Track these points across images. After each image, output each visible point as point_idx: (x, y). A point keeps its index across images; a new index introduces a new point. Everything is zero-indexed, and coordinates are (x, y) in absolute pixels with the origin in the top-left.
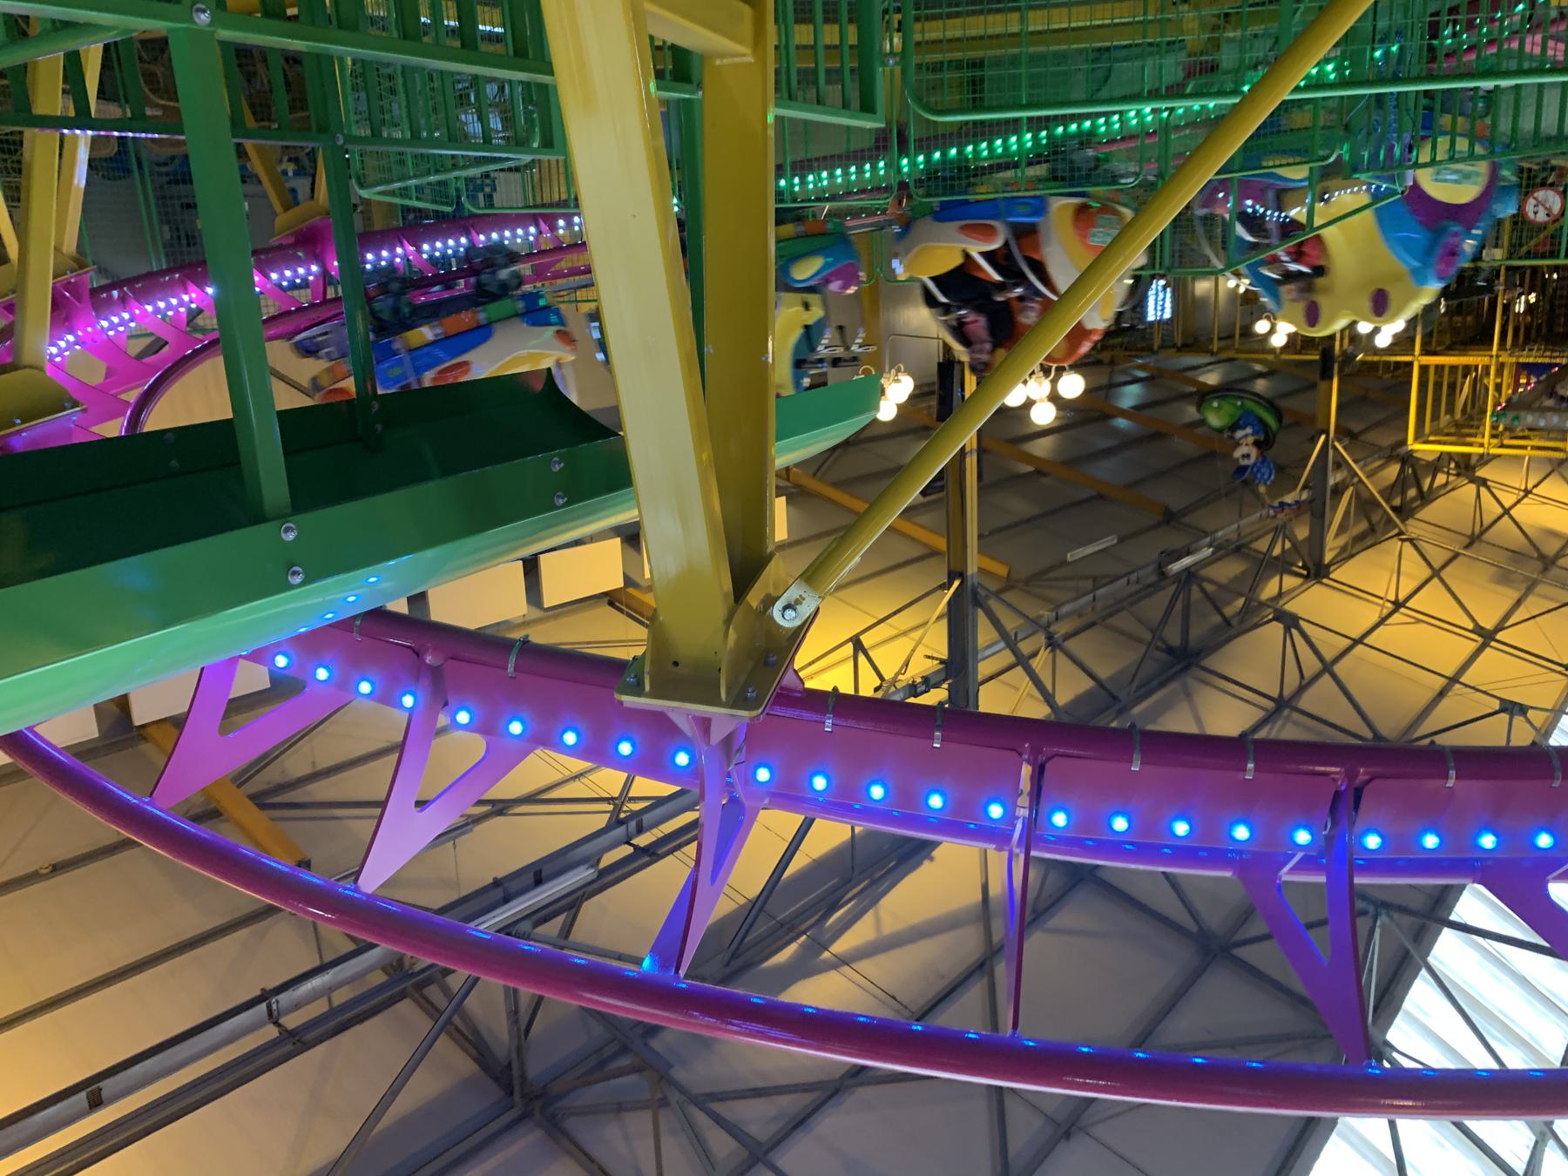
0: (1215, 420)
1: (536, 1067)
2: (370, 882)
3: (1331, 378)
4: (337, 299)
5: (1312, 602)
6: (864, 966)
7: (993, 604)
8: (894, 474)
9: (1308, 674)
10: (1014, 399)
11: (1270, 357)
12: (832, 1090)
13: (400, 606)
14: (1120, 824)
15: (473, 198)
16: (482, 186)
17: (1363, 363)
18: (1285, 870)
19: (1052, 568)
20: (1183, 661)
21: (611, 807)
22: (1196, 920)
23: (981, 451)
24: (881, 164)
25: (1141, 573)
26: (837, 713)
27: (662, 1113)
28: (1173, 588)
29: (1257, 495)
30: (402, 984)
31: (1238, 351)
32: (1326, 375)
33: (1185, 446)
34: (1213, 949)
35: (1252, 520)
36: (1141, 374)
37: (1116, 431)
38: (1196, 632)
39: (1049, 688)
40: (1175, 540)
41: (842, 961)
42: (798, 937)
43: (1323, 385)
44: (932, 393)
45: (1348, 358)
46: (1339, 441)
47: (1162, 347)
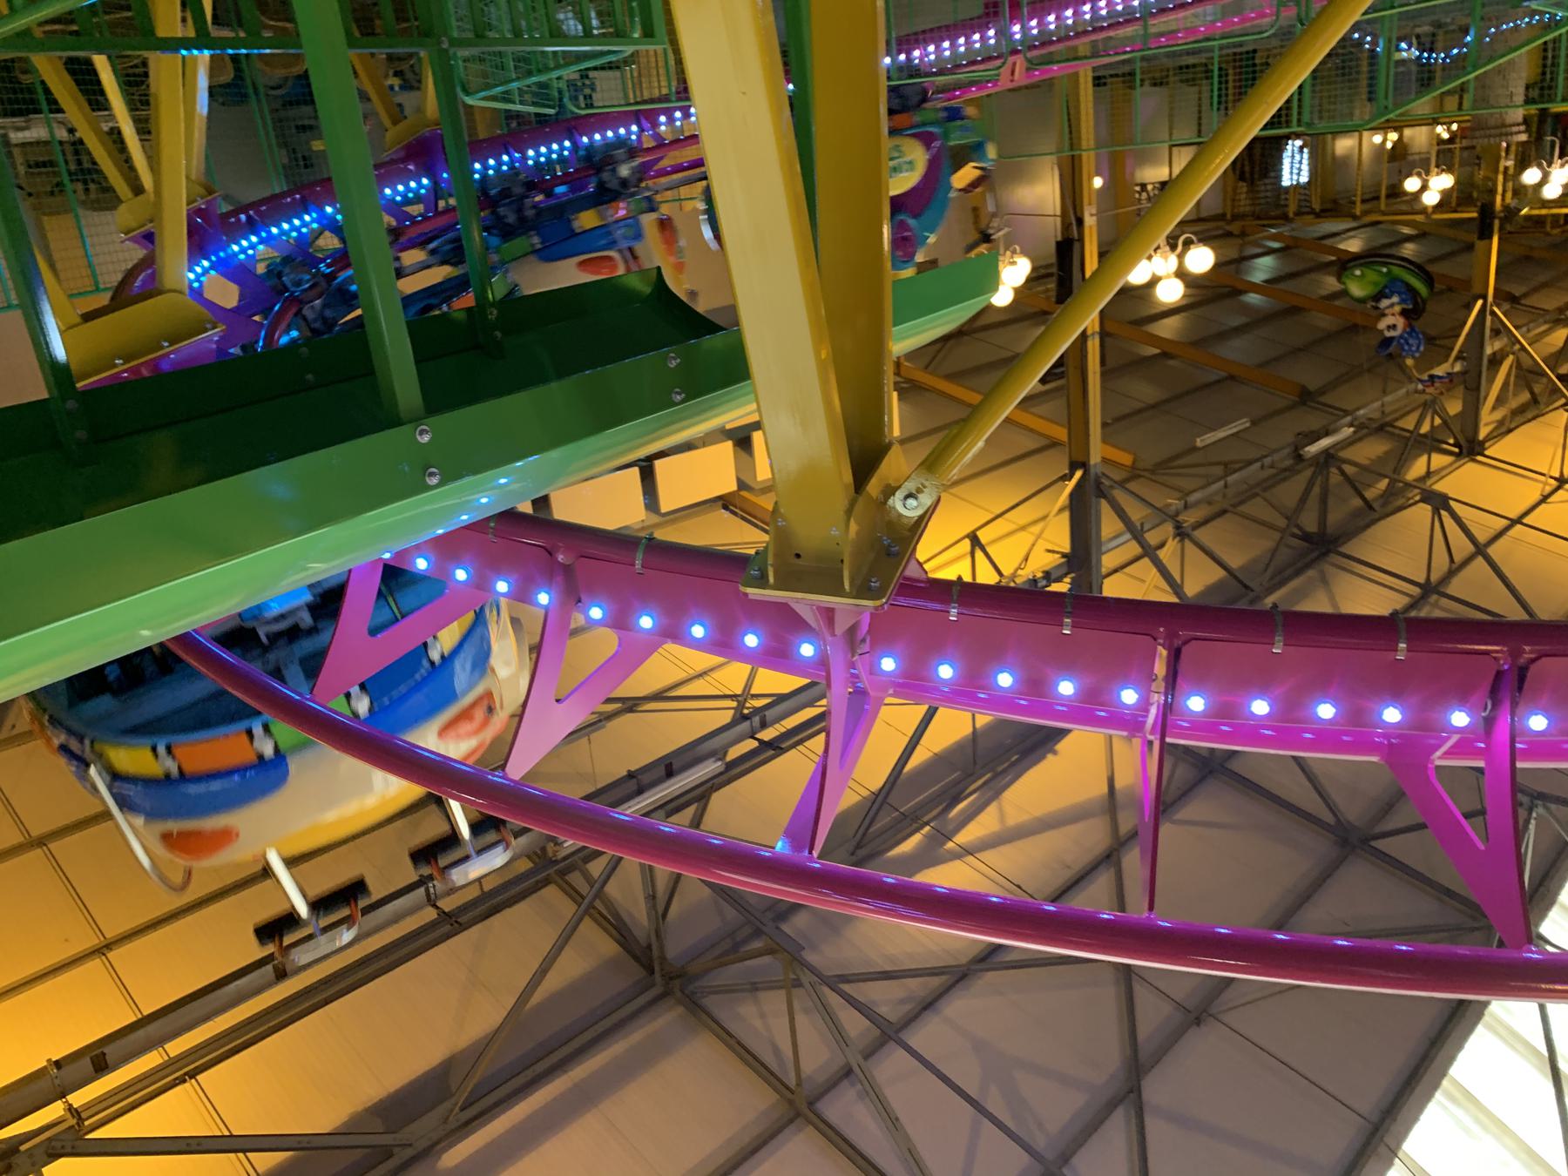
0: (1357, 290)
1: (675, 948)
2: (517, 769)
3: (1491, 238)
4: (450, 210)
5: (1465, 482)
6: (989, 856)
7: (1118, 494)
8: (1009, 363)
9: (1458, 558)
10: (1138, 275)
11: (1420, 218)
12: (958, 976)
13: (526, 508)
14: (1260, 707)
15: (574, 99)
16: (582, 87)
17: (1528, 218)
18: (1438, 754)
19: (1177, 457)
20: (1322, 547)
21: (734, 704)
22: (1335, 815)
23: (1104, 334)
24: (991, 33)
25: (1276, 457)
26: (962, 603)
27: (795, 991)
28: (1308, 473)
29: (1402, 368)
30: (542, 872)
31: (1384, 214)
32: (1485, 234)
33: (1324, 321)
34: (1352, 841)
35: (1395, 397)
36: (1276, 245)
37: (1247, 309)
38: (1335, 517)
39: (1177, 577)
40: (1313, 421)
41: (967, 851)
42: (922, 827)
43: (1480, 245)
44: (1050, 275)
45: (1510, 213)
46: (1499, 306)
47: (1298, 214)
